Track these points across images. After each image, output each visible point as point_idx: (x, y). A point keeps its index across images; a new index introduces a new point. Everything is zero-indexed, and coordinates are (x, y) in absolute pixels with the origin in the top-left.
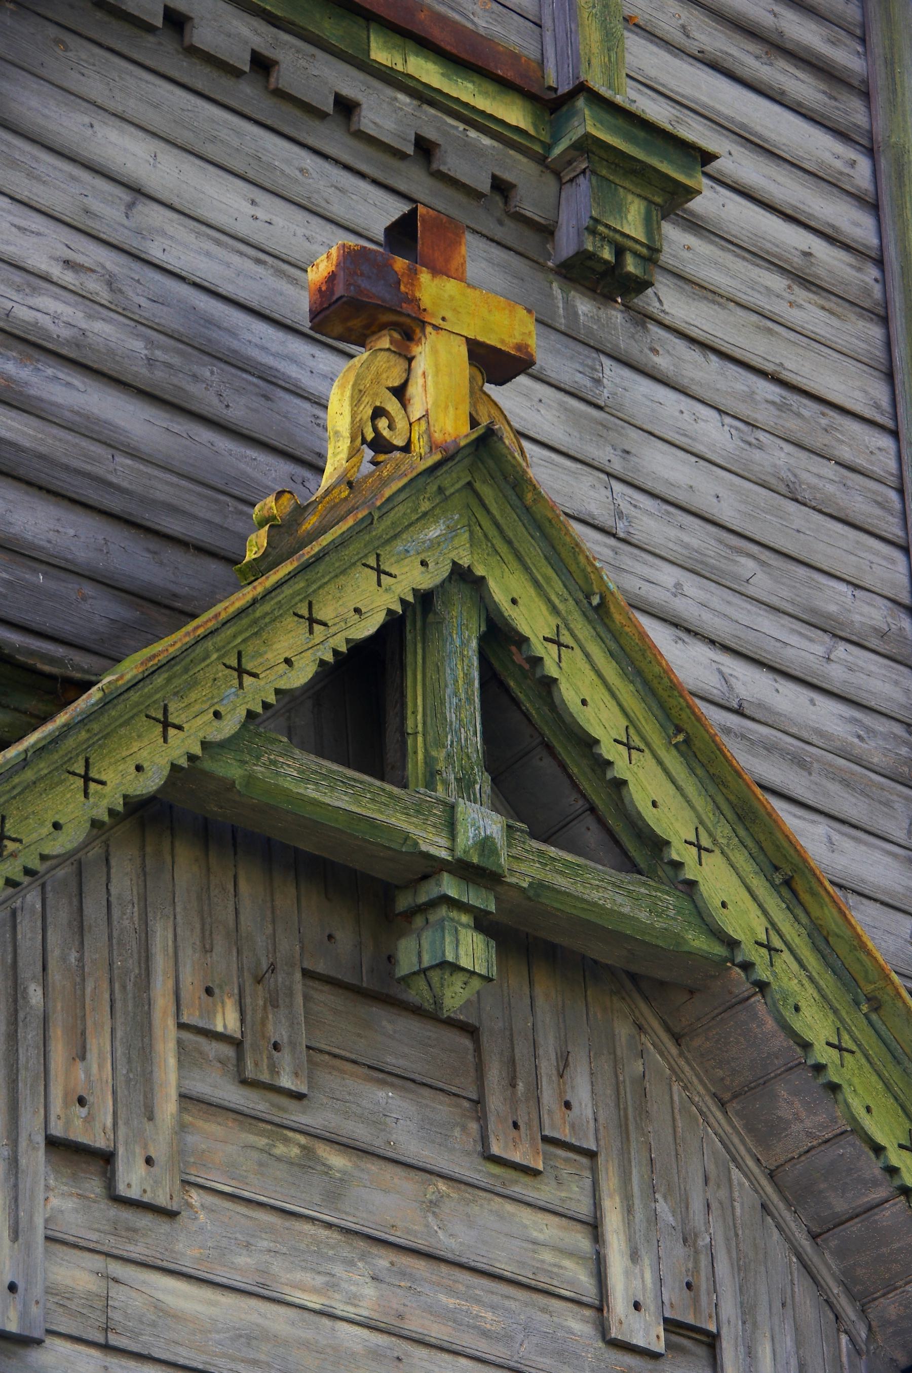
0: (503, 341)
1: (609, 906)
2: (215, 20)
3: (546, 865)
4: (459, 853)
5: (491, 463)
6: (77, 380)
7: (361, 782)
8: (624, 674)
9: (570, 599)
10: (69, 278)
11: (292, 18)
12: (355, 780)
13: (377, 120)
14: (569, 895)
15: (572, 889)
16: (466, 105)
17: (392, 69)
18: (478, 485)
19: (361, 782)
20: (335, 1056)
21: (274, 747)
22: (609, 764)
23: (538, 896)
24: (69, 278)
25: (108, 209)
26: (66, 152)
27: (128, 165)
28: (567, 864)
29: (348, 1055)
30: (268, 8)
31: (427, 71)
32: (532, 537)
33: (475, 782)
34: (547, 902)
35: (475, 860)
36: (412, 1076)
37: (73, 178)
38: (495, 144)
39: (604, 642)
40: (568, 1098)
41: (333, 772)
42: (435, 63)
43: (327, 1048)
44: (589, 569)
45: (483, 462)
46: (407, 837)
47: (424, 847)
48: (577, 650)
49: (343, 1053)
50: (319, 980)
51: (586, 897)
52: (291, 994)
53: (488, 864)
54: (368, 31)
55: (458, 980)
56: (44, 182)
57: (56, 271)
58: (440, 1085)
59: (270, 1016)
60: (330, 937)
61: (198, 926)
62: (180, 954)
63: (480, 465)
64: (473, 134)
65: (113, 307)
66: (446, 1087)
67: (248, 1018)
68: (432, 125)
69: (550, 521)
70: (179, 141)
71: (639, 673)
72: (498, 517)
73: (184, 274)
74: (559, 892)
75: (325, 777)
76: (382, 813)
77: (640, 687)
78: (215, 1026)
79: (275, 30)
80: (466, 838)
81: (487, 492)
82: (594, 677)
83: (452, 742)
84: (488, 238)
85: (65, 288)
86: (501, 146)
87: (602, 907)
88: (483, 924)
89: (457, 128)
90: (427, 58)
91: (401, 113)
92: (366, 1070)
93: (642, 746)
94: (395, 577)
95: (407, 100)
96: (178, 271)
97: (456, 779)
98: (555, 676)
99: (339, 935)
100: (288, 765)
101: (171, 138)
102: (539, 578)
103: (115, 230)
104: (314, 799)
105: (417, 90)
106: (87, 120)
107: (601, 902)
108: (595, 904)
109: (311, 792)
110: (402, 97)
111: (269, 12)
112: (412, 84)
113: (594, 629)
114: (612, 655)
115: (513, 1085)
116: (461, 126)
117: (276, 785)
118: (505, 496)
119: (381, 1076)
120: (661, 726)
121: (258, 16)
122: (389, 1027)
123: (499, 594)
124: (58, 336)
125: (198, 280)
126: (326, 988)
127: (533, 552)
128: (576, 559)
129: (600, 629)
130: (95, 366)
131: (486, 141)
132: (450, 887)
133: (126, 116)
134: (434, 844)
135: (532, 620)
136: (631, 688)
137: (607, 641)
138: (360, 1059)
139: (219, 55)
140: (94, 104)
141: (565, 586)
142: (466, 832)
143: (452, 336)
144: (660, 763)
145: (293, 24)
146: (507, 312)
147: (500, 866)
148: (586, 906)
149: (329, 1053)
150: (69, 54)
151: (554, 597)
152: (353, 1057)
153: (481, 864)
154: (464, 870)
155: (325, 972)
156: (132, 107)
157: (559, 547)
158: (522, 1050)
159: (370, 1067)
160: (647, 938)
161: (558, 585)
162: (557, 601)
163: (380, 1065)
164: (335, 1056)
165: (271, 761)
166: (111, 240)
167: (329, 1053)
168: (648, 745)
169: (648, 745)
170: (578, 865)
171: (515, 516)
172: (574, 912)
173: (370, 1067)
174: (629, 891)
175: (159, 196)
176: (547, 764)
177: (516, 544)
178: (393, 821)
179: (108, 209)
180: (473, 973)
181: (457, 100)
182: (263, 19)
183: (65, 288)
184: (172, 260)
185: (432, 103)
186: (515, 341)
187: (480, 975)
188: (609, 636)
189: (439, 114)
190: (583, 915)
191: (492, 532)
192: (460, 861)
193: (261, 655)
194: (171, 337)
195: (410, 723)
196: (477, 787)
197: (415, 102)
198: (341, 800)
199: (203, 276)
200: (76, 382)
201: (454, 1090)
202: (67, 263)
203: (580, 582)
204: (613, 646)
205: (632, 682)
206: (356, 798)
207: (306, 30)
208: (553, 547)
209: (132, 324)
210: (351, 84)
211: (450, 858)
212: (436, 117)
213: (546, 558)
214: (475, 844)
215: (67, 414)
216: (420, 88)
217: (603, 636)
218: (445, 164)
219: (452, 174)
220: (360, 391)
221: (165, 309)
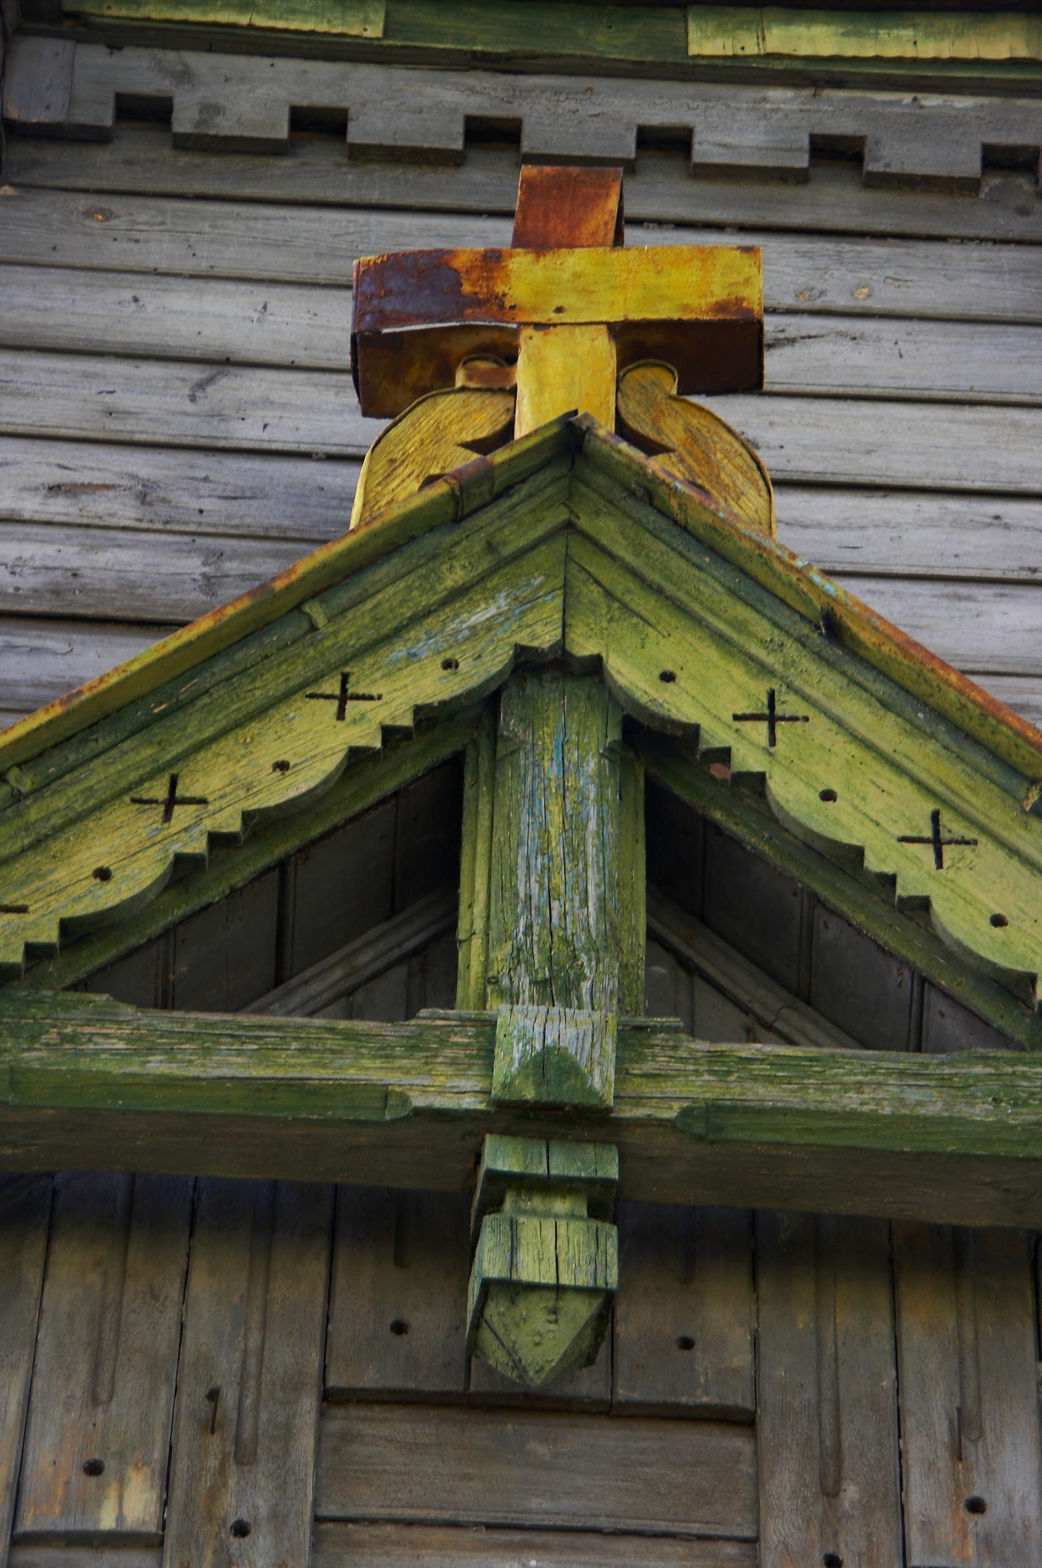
0: (685, 308)
1: (887, 1111)
2: (390, 99)
3: (729, 1073)
4: (496, 1092)
5: (601, 480)
6: (55, 640)
7: (271, 1027)
8: (915, 729)
9: (789, 643)
10: (59, 507)
11: (528, 48)
12: (262, 1027)
13: (728, 140)
14: (785, 1112)
15: (794, 1101)
16: (899, 61)
17: (735, 57)
18: (584, 523)
19: (271, 1027)
20: (410, 1523)
21: (75, 1013)
22: (891, 880)
23: (720, 1129)
24: (59, 507)
25: (156, 400)
26: (81, 345)
27: (206, 332)
28: (779, 1062)
29: (433, 1514)
30: (479, 48)
31: (812, 39)
32: (699, 568)
33: (581, 977)
34: (740, 1135)
35: (529, 1094)
36: (591, 1523)
37: (86, 375)
38: (985, 101)
39: (866, 690)
40: (976, 1493)
41: (213, 1025)
42: (826, 23)
43: (385, 1512)
44: (794, 578)
45: (587, 484)
46: (385, 1094)
47: (419, 1101)
48: (819, 722)
49: (421, 1514)
50: (381, 1403)
51: (827, 1106)
52: (287, 1433)
53: (566, 1094)
54: (686, 21)
55: (534, 1313)
56: (27, 394)
57: (31, 506)
58: (662, 1526)
59: (232, 1482)
60: (399, 1328)
61: (83, 1368)
62: (36, 1420)
63: (583, 489)
64: (932, 101)
65: (145, 525)
66: (674, 1528)
67: (178, 1495)
68: (837, 113)
69: (716, 530)
70: (323, 278)
71: (940, 716)
72: (629, 558)
73: (303, 448)
74: (762, 1112)
75: (191, 1037)
76: (324, 1066)
77: (947, 739)
78: (98, 1521)
79: (510, 78)
80: (510, 1059)
81: (606, 528)
82: (854, 749)
83: (529, 927)
84: (995, 242)
85: (49, 523)
86: (996, 100)
87: (873, 1117)
88: (602, 1202)
89: (898, 103)
90: (810, 22)
91: (775, 116)
92: (483, 1535)
93: (971, 834)
94: (380, 697)
95: (790, 93)
96: (293, 447)
97: (534, 982)
98: (756, 768)
99: (416, 1319)
100: (107, 1036)
101: (306, 277)
102: (723, 627)
103: (168, 423)
104: (161, 1076)
105: (799, 73)
106: (127, 295)
107: (866, 1109)
108: (853, 1115)
109: (157, 1066)
110: (777, 94)
111: (483, 53)
112: (779, 66)
113: (843, 673)
114: (885, 705)
115: (831, 1492)
116: (907, 98)
117: (74, 1073)
118: (638, 522)
119: (517, 1537)
120: (1004, 790)
121: (475, 68)
122: (542, 1450)
123: (630, 674)
124: (17, 589)
125: (334, 450)
126: (399, 1413)
127: (708, 589)
128: (772, 570)
129: (851, 669)
130: (90, 612)
131: (963, 103)
132: (502, 1157)
133: (217, 271)
134: (457, 1091)
135: (704, 692)
136: (932, 746)
137: (869, 685)
138: (463, 1517)
139: (401, 143)
140: (156, 272)
141: (775, 624)
142: (508, 1052)
143: (578, 330)
144: (1014, 852)
145: (534, 56)
146: (696, 263)
147: (591, 1092)
148: (833, 1124)
149: (395, 1521)
150: (113, 223)
151: (755, 649)
152: (446, 1515)
153: (545, 1098)
154: (515, 1117)
155: (380, 1385)
156: (229, 258)
157: (742, 560)
158: (859, 1432)
159: (490, 1527)
160: (1002, 1150)
161: (762, 628)
162: (761, 654)
163: (512, 1518)
164: (410, 1523)
165: (64, 1038)
166: (162, 439)
167: (395, 1521)
168: (984, 830)
169: (984, 830)
170: (811, 1059)
171: (663, 547)
172: (807, 1139)
173: (490, 1527)
174: (942, 1078)
175: (253, 357)
176: (834, 925)
177: (669, 588)
178: (352, 1073)
179: (156, 400)
180: (559, 1289)
181: (878, 60)
182: (486, 70)
183: (49, 523)
184: (281, 437)
185: (838, 83)
186: (714, 300)
187: (578, 1290)
188: (871, 676)
189: (858, 94)
190: (837, 1141)
191: (620, 584)
192: (501, 1106)
193: (42, 877)
194: (266, 538)
195: (463, 926)
196: (585, 986)
197: (806, 93)
198: (232, 1064)
199: (345, 441)
200: (50, 644)
201: (696, 1528)
202: (55, 489)
203: (798, 607)
204: (879, 688)
205: (932, 736)
206: (263, 1056)
207: (560, 56)
208: (742, 571)
209: (187, 539)
210: (662, 106)
211: (482, 1107)
212: (850, 100)
213: (732, 592)
214: (523, 1067)
215: (24, 690)
216: (799, 66)
217: (860, 679)
218: (877, 159)
219: (894, 169)
220: (392, 461)
221: (255, 503)
